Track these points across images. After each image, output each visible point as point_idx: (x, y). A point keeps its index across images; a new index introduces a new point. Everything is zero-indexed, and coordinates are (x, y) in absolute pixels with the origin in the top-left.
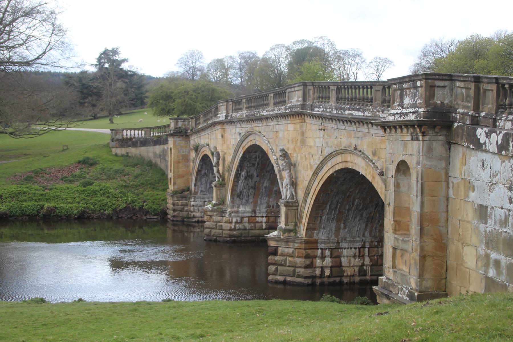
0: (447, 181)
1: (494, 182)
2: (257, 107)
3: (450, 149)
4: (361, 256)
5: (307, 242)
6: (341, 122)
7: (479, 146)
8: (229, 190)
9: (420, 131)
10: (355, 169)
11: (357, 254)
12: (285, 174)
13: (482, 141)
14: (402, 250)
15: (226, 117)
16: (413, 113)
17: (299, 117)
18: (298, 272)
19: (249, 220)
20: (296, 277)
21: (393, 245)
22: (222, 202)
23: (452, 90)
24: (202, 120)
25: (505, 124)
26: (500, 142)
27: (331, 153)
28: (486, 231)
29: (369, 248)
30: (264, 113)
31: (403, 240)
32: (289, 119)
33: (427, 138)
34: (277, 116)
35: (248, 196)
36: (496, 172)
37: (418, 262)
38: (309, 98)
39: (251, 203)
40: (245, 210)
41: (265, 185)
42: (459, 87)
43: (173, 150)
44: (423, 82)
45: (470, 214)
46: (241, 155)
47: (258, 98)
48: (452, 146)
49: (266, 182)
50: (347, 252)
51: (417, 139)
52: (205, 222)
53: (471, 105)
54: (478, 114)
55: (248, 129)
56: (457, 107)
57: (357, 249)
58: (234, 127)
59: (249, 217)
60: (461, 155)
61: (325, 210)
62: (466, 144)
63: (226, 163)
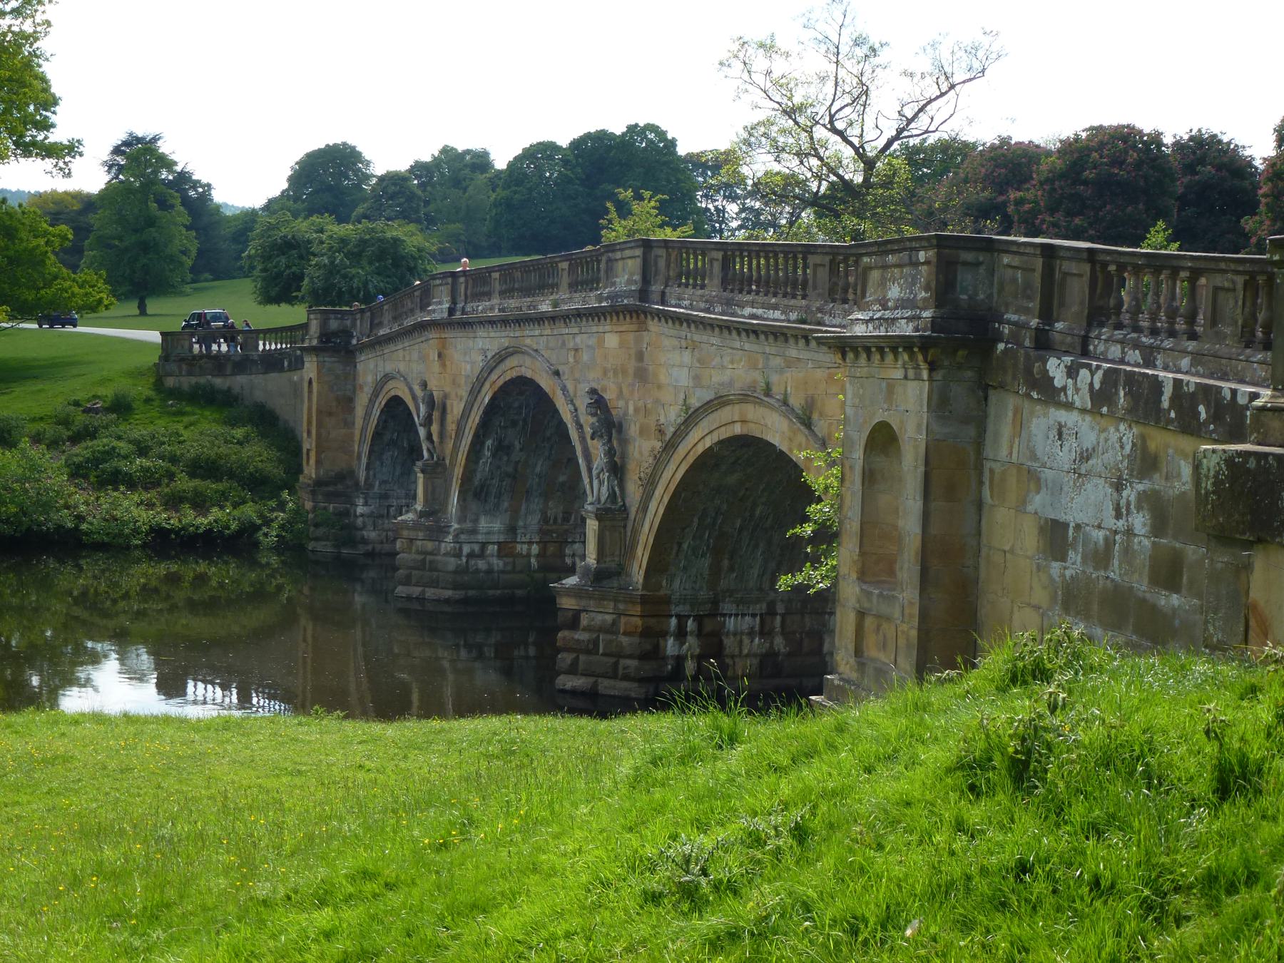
0: (979, 468)
1: (1083, 472)
2: (528, 291)
3: (986, 399)
4: (765, 632)
5: (644, 600)
6: (734, 333)
7: (1050, 394)
8: (454, 480)
9: (925, 360)
10: (765, 438)
11: (757, 628)
12: (598, 449)
13: (1058, 383)
14: (878, 616)
15: (451, 311)
16: (909, 319)
17: (631, 317)
18: (625, 668)
19: (499, 550)
20: (621, 680)
21: (858, 605)
22: (434, 510)
23: (991, 272)
24: (387, 317)
25: (1107, 350)
26: (1097, 386)
27: (708, 402)
28: (1063, 576)
29: (783, 616)
30: (545, 307)
31: (880, 595)
32: (608, 321)
33: (939, 375)
34: (578, 314)
35: (499, 496)
36: (1087, 450)
37: (916, 642)
38: (655, 275)
39: (506, 511)
40: (491, 526)
41: (538, 469)
42: (1009, 266)
43: (315, 385)
44: (931, 253)
45: (1030, 541)
46: (487, 400)
47: (530, 271)
48: (991, 392)
49: (540, 463)
50: (735, 624)
51: (918, 378)
52: (398, 554)
53: (1035, 305)
54: (1049, 325)
55: (506, 342)
56: (1003, 309)
57: (758, 619)
58: (471, 335)
59: (499, 543)
60: (1010, 414)
61: (688, 529)
62: (1023, 390)
63: (449, 418)
